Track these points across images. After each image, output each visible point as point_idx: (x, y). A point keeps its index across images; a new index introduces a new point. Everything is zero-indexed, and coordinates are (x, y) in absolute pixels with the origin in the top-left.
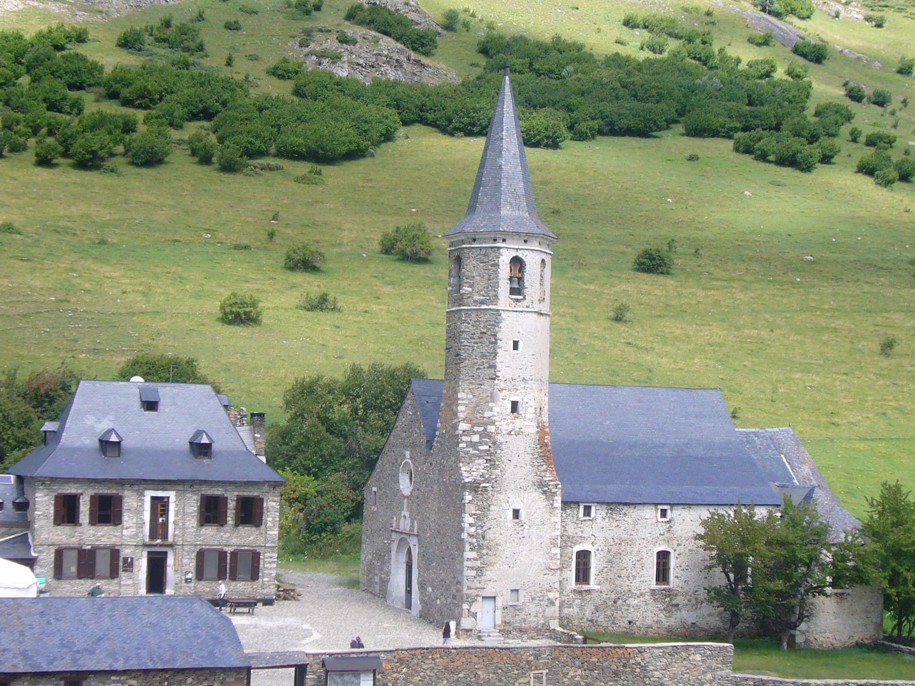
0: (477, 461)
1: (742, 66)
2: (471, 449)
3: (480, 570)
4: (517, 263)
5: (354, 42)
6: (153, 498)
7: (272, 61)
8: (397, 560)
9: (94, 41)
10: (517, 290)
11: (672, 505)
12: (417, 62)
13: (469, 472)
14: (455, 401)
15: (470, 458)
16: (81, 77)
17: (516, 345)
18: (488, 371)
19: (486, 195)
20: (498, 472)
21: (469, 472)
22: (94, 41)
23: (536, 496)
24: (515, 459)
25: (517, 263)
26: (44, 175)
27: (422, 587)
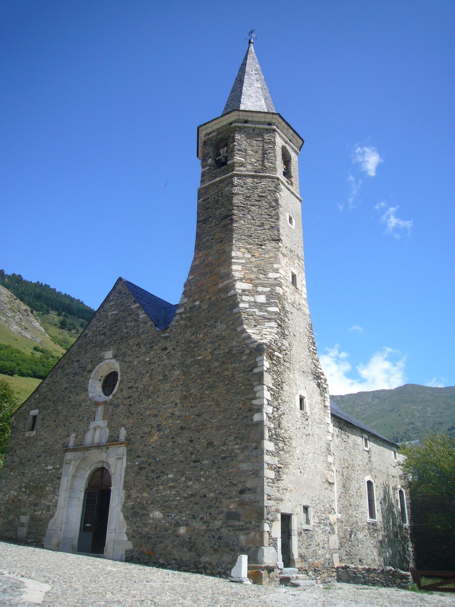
0: (267, 324)
2: (256, 310)
3: (278, 470)
8: (72, 488)
10: (287, 173)
14: (228, 260)
27: (135, 514)
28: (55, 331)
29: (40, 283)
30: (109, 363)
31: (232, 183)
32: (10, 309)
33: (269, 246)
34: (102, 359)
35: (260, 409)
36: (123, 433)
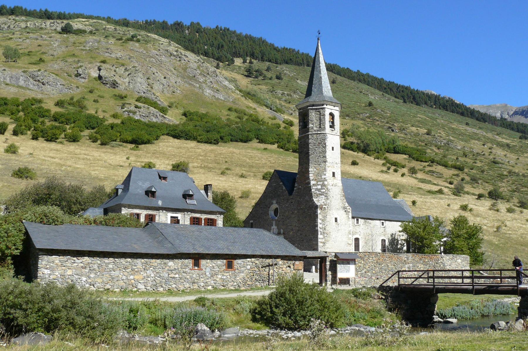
1: (270, 124)
3: (324, 243)
4: (331, 115)
5: (141, 108)
6: (172, 217)
7: (112, 113)
9: (45, 103)
10: (332, 126)
11: (385, 220)
12: (163, 116)
13: (318, 201)
15: (317, 195)
16: (44, 113)
17: (333, 148)
18: (322, 159)
19: (316, 88)
20: (328, 201)
21: (318, 201)
22: (45, 103)
23: (343, 212)
24: (335, 196)
25: (331, 115)
26: (34, 143)
28: (244, 82)
29: (219, 27)
30: (275, 206)
31: (308, 138)
32: (200, 74)
33: (323, 164)
34: (272, 204)
35: (317, 226)
36: (282, 231)
